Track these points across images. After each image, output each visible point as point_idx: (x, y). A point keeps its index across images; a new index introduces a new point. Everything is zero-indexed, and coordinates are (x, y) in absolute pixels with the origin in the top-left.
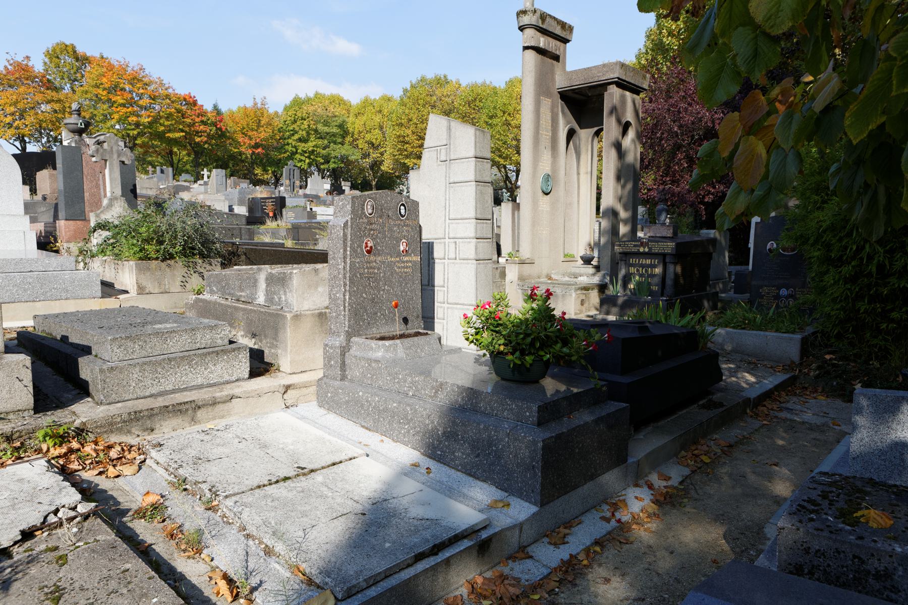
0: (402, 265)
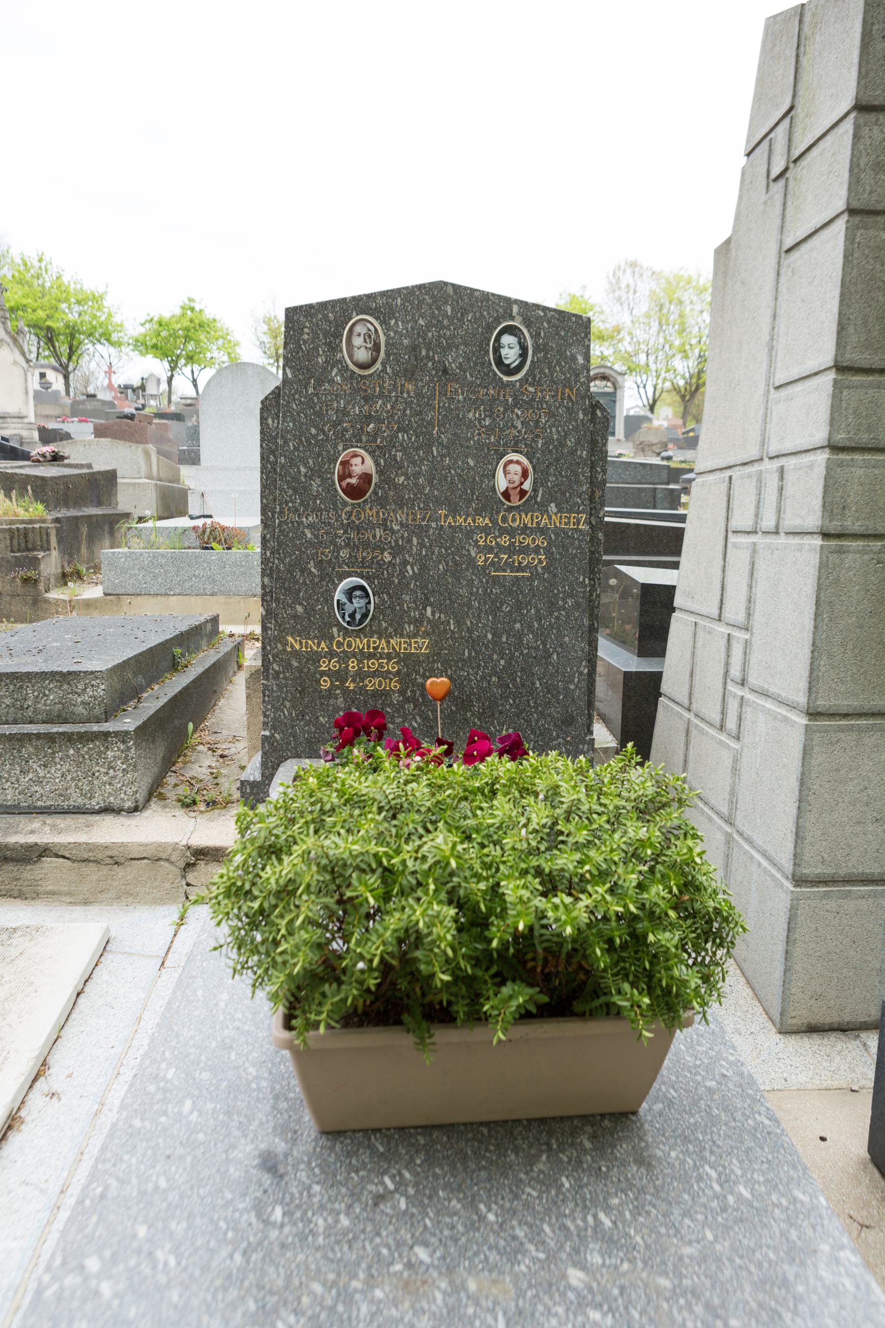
0: (504, 541)
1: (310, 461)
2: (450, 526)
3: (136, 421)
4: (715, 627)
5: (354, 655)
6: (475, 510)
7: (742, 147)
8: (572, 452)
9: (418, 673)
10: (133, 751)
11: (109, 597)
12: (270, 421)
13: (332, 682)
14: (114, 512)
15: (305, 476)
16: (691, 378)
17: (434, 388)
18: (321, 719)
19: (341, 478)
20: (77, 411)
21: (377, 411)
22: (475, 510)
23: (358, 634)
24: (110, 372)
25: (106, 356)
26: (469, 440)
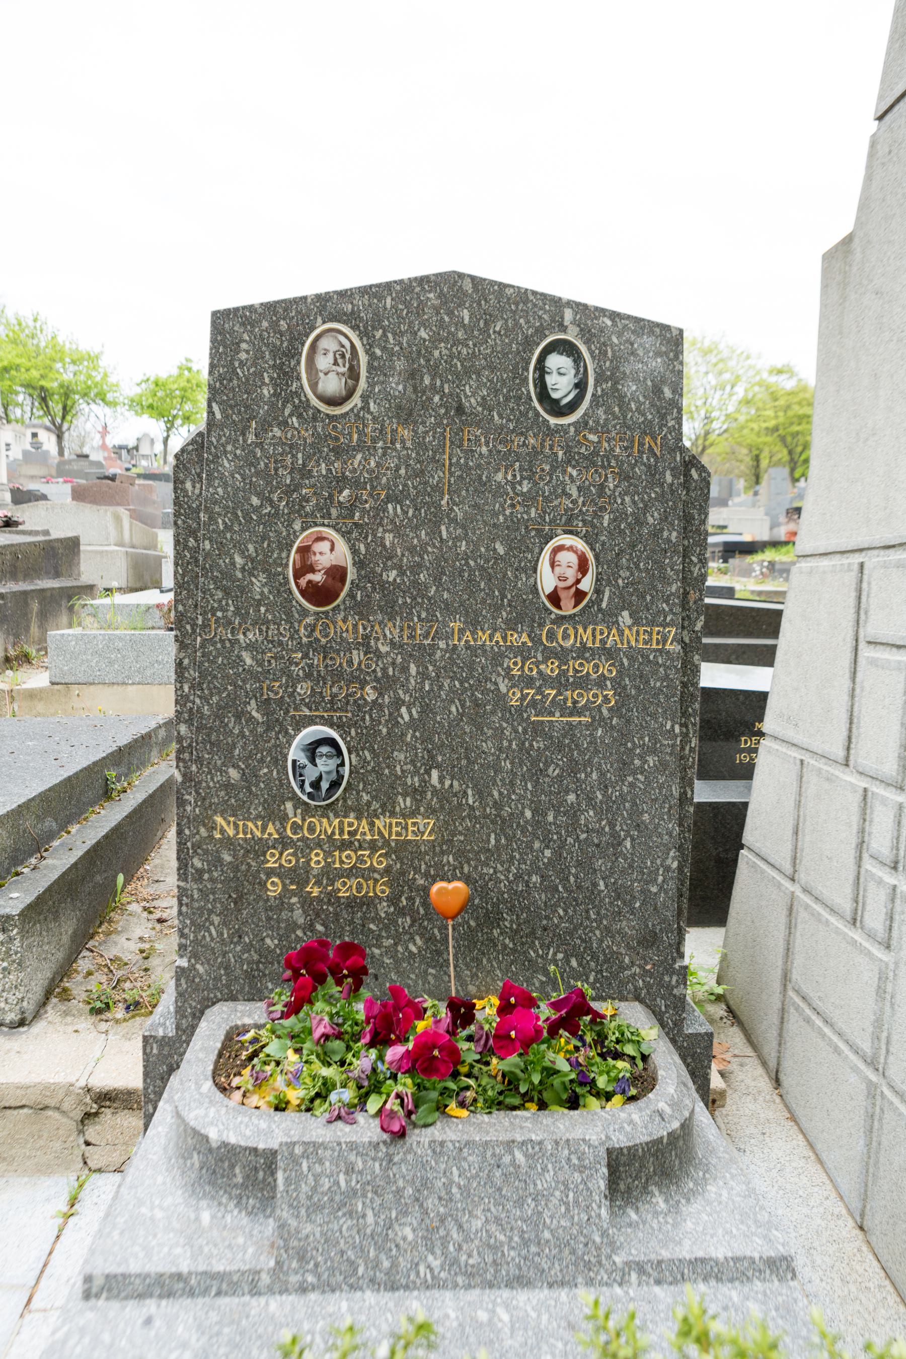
0: (551, 668)
1: (251, 547)
2: (468, 647)
3: (118, 482)
4: (837, 773)
5: (319, 845)
6: (507, 622)
7: (870, 106)
8: (656, 534)
9: (417, 870)
10: (17, 943)
11: (56, 687)
12: (188, 485)
13: (284, 885)
14: (75, 584)
15: (243, 569)
16: (697, 439)
17: (443, 434)
18: (268, 941)
19: (297, 575)
20: (62, 471)
21: (354, 470)
22: (507, 622)
23: (325, 811)
24: (105, 431)
25: (102, 417)
26: (496, 514)
